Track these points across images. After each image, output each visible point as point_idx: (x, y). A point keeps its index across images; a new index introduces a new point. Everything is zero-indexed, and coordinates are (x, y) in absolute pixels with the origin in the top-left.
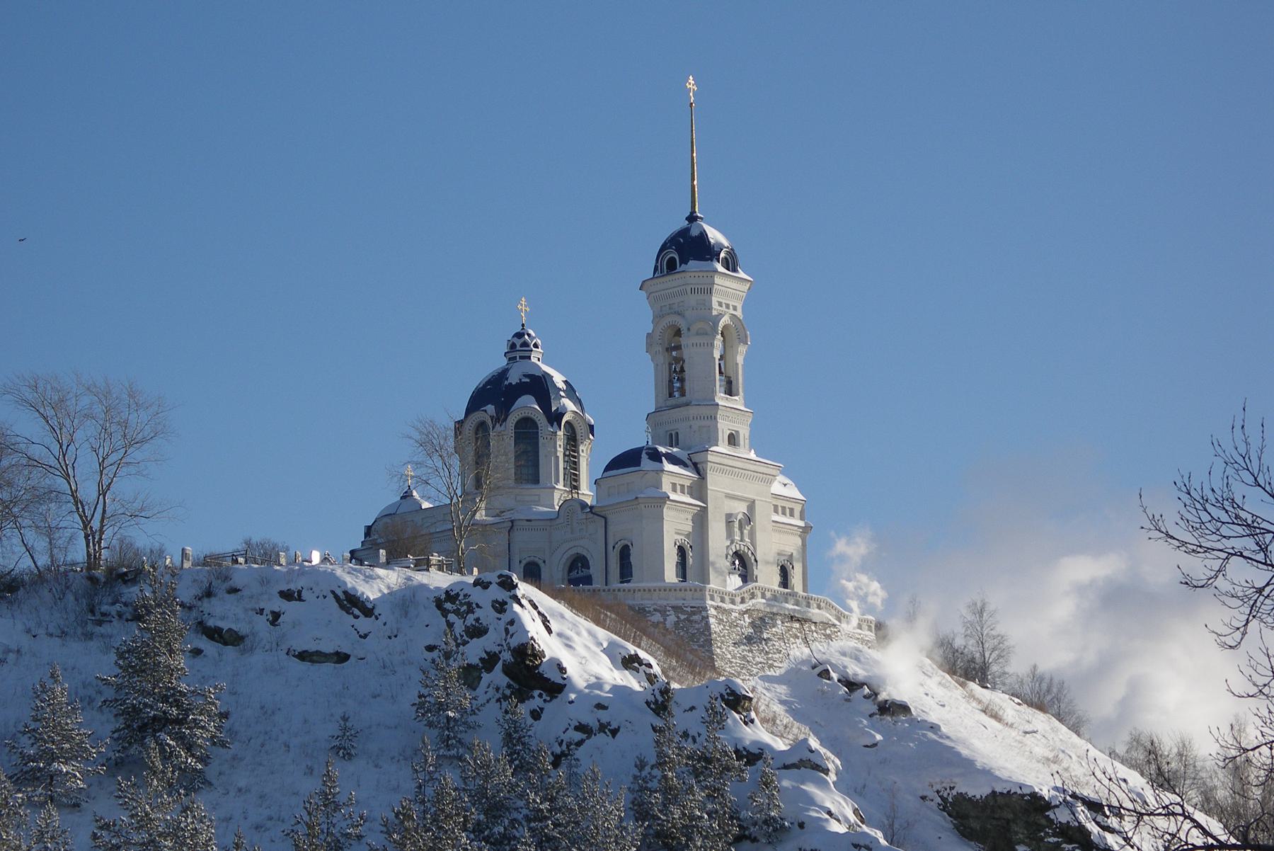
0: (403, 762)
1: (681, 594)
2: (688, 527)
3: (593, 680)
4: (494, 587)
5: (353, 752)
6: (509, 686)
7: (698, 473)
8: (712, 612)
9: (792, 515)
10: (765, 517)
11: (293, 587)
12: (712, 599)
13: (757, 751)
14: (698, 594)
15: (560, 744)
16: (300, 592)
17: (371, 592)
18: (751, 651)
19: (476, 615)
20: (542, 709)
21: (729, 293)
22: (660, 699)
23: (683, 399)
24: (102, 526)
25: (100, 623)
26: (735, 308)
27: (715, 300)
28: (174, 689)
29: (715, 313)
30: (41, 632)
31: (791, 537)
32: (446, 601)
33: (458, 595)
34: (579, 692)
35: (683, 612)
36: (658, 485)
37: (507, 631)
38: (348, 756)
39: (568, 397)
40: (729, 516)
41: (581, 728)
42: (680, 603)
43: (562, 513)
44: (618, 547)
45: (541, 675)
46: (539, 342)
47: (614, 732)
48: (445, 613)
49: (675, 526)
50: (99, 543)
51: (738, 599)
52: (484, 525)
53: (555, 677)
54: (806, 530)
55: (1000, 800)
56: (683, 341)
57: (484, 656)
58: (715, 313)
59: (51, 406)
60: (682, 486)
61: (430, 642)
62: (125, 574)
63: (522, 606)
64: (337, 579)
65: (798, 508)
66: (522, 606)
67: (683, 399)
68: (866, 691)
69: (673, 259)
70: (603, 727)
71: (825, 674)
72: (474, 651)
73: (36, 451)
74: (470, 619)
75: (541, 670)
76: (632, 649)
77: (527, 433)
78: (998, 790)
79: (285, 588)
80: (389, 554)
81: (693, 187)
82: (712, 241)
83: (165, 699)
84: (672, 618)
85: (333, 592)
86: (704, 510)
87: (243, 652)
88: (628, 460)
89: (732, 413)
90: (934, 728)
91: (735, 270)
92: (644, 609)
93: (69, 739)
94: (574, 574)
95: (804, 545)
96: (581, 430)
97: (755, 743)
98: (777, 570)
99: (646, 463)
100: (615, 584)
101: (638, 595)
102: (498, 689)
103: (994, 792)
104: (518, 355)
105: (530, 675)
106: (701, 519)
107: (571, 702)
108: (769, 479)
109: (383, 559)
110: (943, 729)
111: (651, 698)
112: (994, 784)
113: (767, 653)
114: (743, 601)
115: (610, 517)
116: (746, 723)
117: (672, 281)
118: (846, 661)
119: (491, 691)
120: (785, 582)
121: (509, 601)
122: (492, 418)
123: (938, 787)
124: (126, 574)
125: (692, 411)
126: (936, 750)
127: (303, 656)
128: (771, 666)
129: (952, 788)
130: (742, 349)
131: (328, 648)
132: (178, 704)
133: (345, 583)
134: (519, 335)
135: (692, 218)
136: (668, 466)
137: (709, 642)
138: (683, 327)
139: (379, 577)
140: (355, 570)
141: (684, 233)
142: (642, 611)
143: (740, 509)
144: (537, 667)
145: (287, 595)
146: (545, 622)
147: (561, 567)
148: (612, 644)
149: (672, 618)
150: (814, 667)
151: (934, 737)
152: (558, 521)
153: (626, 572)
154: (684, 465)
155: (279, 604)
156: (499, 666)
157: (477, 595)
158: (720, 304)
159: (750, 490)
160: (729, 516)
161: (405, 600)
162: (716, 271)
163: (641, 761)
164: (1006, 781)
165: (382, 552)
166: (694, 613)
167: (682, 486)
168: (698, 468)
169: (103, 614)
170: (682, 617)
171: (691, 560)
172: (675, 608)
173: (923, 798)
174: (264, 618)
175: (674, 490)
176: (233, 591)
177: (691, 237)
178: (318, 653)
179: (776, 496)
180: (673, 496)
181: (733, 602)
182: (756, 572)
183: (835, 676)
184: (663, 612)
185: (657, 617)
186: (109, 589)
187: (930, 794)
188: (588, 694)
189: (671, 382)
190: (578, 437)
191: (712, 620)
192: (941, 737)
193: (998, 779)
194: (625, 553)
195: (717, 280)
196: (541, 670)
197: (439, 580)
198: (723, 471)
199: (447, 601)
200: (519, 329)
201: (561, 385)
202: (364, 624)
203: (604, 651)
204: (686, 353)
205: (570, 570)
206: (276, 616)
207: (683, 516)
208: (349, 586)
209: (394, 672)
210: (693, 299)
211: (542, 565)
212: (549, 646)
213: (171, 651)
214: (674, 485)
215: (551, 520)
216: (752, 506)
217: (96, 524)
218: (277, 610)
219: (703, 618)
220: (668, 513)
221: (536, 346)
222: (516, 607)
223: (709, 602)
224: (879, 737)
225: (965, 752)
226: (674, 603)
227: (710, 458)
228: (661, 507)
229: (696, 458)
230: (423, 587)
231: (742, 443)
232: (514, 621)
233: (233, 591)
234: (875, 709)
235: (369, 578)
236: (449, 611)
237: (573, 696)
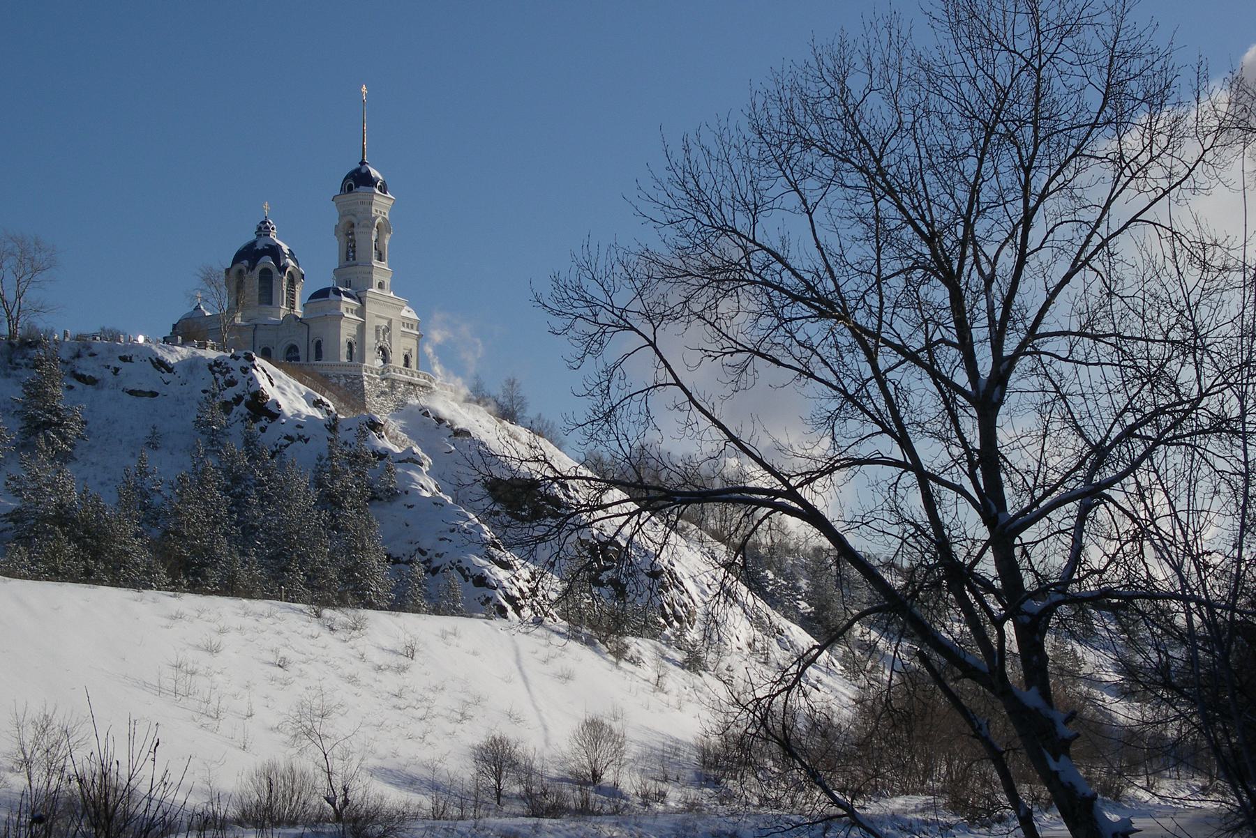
10: (397, 328)
17: (172, 359)
21: (382, 205)
27: (373, 208)
41: (287, 437)
47: (306, 441)
49: (347, 331)
53: (275, 410)
70: (300, 438)
72: (229, 394)
76: (319, 396)
83: (50, 412)
84: (343, 381)
88: (322, 294)
89: (381, 270)
90: (483, 444)
96: (297, 277)
105: (261, 408)
106: (362, 328)
117: (350, 197)
120: (407, 365)
125: (359, 269)
127: (132, 393)
130: (388, 236)
134: (264, 223)
135: (363, 163)
136: (344, 299)
137: (363, 395)
141: (358, 170)
142: (326, 377)
143: (384, 323)
145: (124, 359)
148: (308, 393)
153: (319, 356)
154: (353, 298)
155: (118, 364)
159: (390, 314)
161: (191, 365)
171: (356, 350)
176: (93, 355)
179: (404, 317)
184: (338, 377)
194: (318, 345)
197: (211, 354)
199: (215, 366)
202: (167, 376)
206: (117, 370)
215: (278, 325)
216: (390, 322)
217: (14, 314)
230: (202, 357)
232: (253, 378)
233: (93, 355)
235: (171, 351)
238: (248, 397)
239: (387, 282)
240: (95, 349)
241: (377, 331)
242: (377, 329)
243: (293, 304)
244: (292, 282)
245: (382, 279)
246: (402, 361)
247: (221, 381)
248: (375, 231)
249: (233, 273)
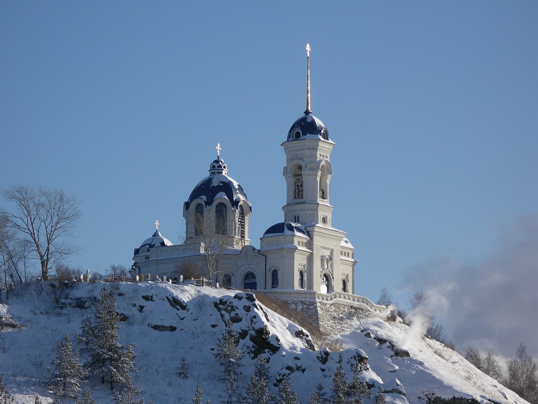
0: (209, 381)
1: (304, 296)
2: (305, 262)
3: (291, 345)
4: (244, 300)
5: (188, 375)
6: (253, 347)
7: (309, 236)
8: (319, 304)
9: (348, 256)
10: (338, 257)
11: (149, 294)
12: (318, 299)
13: (372, 383)
14: (312, 296)
15: (280, 375)
16: (152, 297)
17: (185, 298)
18: (335, 323)
19: (236, 312)
20: (269, 358)
21: (324, 150)
22: (324, 356)
23: (302, 200)
24: (47, 258)
25: (62, 308)
26: (327, 157)
27: (318, 153)
28: (114, 345)
29: (318, 160)
30: (38, 312)
31: (348, 267)
32: (220, 304)
33: (226, 302)
34: (286, 351)
35: (305, 304)
36: (292, 242)
37: (252, 321)
38: (185, 377)
39: (240, 193)
40: (322, 257)
41: (289, 368)
42: (304, 300)
43: (243, 251)
44: (271, 270)
45: (269, 342)
46: (226, 166)
47: (303, 371)
48: (219, 310)
49: (299, 261)
50: (47, 265)
51: (329, 298)
52: (204, 256)
53: (275, 344)
54: (354, 263)
55: (457, 401)
56: (303, 172)
57: (241, 331)
58: (318, 160)
59: (21, 197)
60: (302, 242)
61: (213, 323)
62: (67, 283)
63: (258, 309)
64: (169, 291)
65: (351, 253)
66: (258, 309)
67: (302, 200)
68: (388, 344)
69: (298, 133)
70: (298, 368)
71: (368, 335)
72: (236, 328)
73: (19, 222)
74: (233, 314)
75: (269, 340)
76: (300, 328)
77: (221, 209)
78: (456, 396)
79: (145, 295)
80: (184, 278)
81: (308, 97)
82: (317, 125)
83: (110, 350)
84: (300, 307)
85: (167, 297)
86: (312, 254)
87: (129, 324)
88: (277, 229)
89: (325, 207)
90: (421, 364)
91: (327, 139)
92: (287, 302)
93: (73, 367)
94: (247, 281)
95: (353, 270)
96: (246, 209)
97: (371, 380)
98: (341, 283)
99: (287, 232)
100: (269, 289)
101: (284, 295)
102: (248, 348)
103: (454, 397)
104: (216, 171)
105: (263, 342)
106: (310, 259)
107: (284, 356)
108: (339, 239)
109: (182, 280)
110: (425, 364)
111: (319, 355)
112: (454, 394)
113: (342, 324)
114: (331, 299)
115: (268, 256)
116: (365, 370)
117: (297, 144)
118: (376, 328)
119: (245, 348)
120: (345, 289)
121: (252, 306)
122: (205, 202)
123: (427, 393)
124: (65, 283)
125: (307, 206)
126: (426, 377)
127: (156, 327)
128: (343, 330)
129: (433, 394)
130: (329, 176)
131: (167, 324)
132: (116, 352)
133: (173, 293)
134: (217, 162)
135: (307, 112)
136: (297, 233)
137: (317, 319)
138: (303, 166)
139: (187, 291)
140: (175, 287)
141: (303, 120)
142: (286, 303)
143: (327, 253)
144: (267, 339)
145: (146, 298)
146: (266, 316)
147: (241, 277)
148: (290, 325)
149: (300, 307)
150: (362, 331)
151: (422, 368)
152: (240, 256)
153: (275, 283)
154: (304, 233)
155: (143, 302)
156: (248, 337)
157: (236, 303)
158: (320, 155)
159: (331, 244)
160: (322, 257)
161: (201, 301)
162: (320, 140)
163: (320, 386)
164: (460, 393)
165: (182, 276)
166: (310, 305)
167: (302, 242)
168: (309, 234)
169: (62, 304)
170: (305, 306)
171: (306, 276)
172: (301, 302)
173: (419, 398)
174: (136, 308)
175: (299, 245)
176: (121, 295)
177: (308, 122)
178: (163, 326)
179: (342, 247)
180: (299, 248)
181: (327, 300)
182: (333, 284)
183: (372, 336)
184: (296, 304)
185: (293, 306)
186: (60, 290)
187: (423, 396)
188: (290, 352)
189: (295, 191)
190: (245, 213)
191: (318, 308)
192: (425, 368)
193: (456, 391)
194: (275, 274)
195: (320, 144)
196: (269, 340)
197: (216, 292)
198: (320, 236)
199: (221, 304)
200: (216, 159)
201: (237, 187)
202: (182, 313)
203: (287, 328)
204: (305, 178)
205: (245, 279)
206: (142, 308)
207: (302, 257)
208: (175, 295)
209: (198, 337)
210: (308, 152)
211: (232, 276)
212: (272, 331)
213: (113, 328)
214: (299, 242)
215: (237, 254)
216: (332, 252)
217: (45, 258)
218: (142, 305)
219: (315, 307)
220: (297, 256)
221: (225, 167)
222: (256, 310)
223: (317, 300)
224: (397, 367)
225: (437, 376)
226: (301, 299)
227: (315, 229)
228: (294, 253)
229: (308, 229)
230: (206, 296)
231: (328, 222)
232: (255, 316)
233: (121, 295)
234: (393, 353)
235: (183, 291)
236: (222, 309)
237: (284, 353)
238: (253, 333)
239: (329, 217)
240: (123, 290)
241: (322, 260)
242: (322, 258)
243: (249, 235)
244: (242, 215)
245: (325, 214)
246: (341, 286)
247: (227, 317)
248: (319, 173)
249: (193, 206)
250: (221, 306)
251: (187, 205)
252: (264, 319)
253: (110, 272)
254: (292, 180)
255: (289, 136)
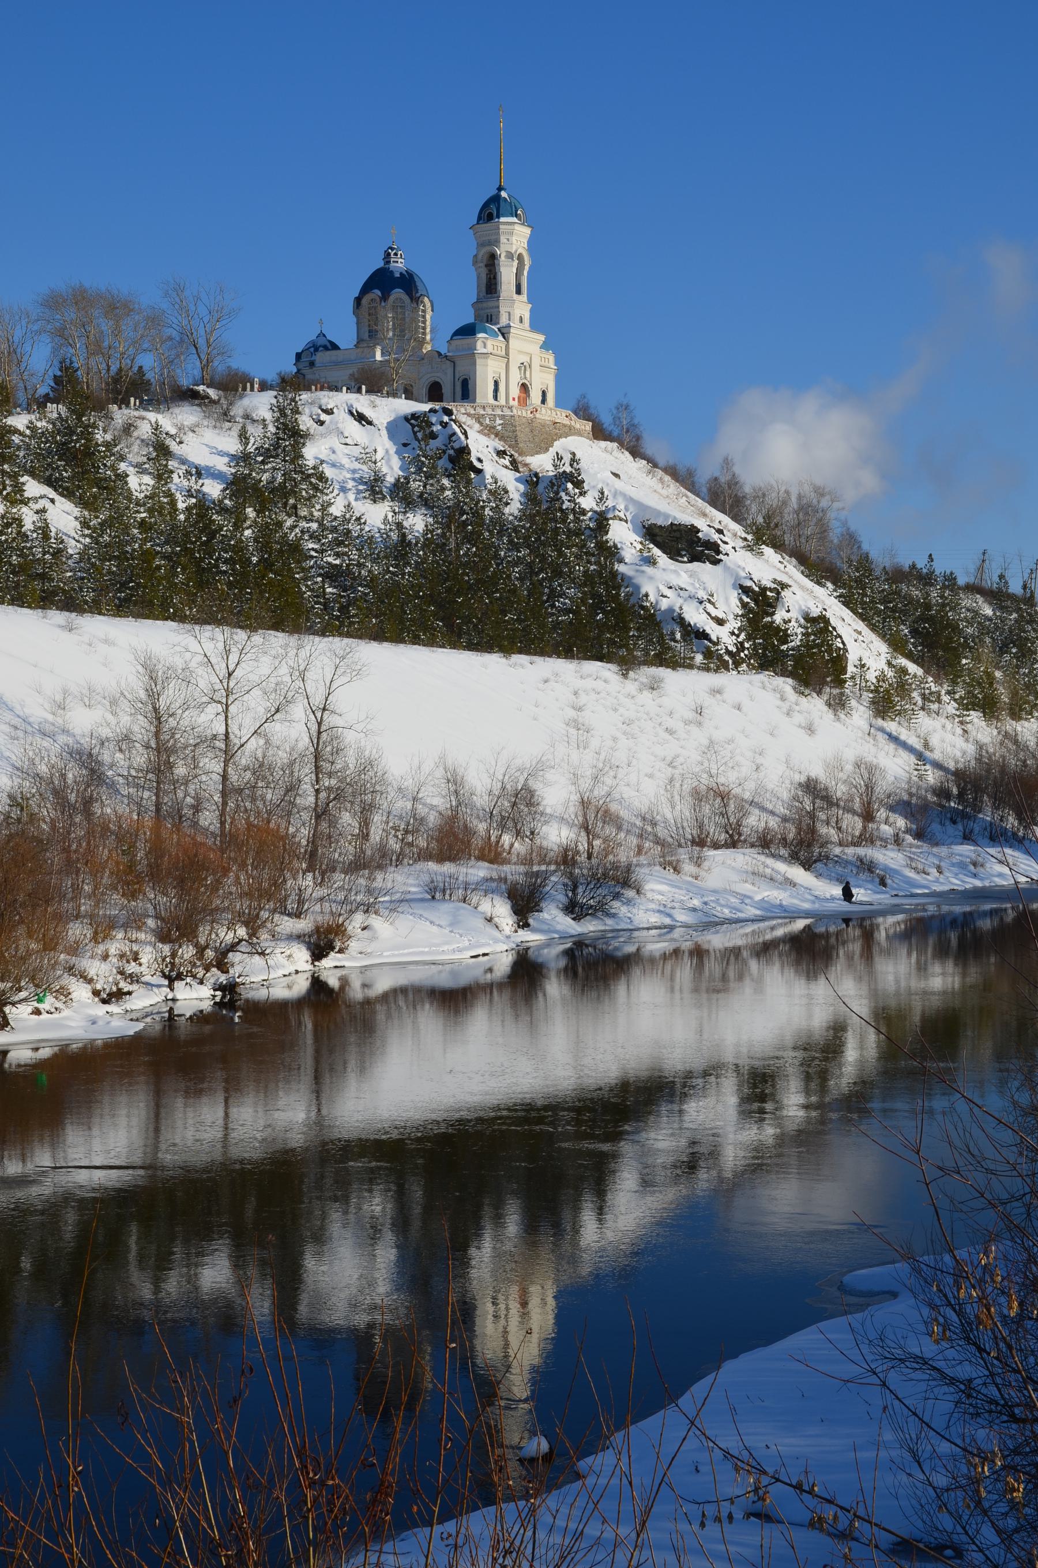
115: (458, 363)
120: (543, 401)
249: (365, 301)
250: (413, 421)
251: (358, 301)
252: (463, 437)
253: (436, 801)
254: (484, 271)
255: (479, 218)
